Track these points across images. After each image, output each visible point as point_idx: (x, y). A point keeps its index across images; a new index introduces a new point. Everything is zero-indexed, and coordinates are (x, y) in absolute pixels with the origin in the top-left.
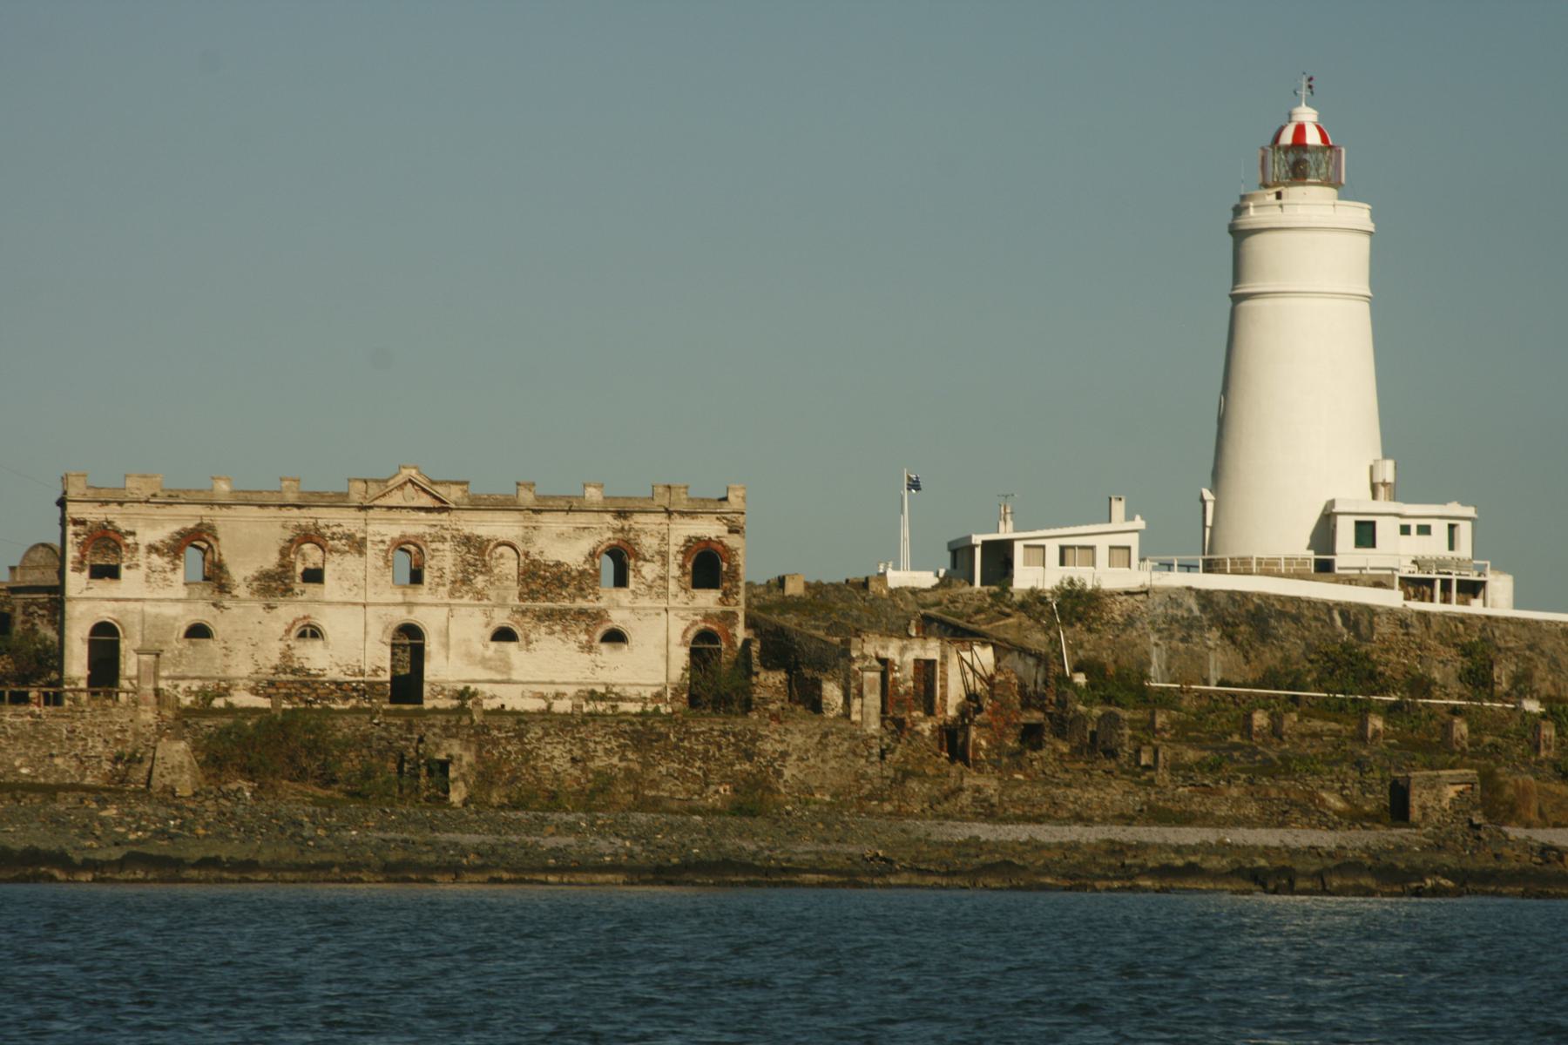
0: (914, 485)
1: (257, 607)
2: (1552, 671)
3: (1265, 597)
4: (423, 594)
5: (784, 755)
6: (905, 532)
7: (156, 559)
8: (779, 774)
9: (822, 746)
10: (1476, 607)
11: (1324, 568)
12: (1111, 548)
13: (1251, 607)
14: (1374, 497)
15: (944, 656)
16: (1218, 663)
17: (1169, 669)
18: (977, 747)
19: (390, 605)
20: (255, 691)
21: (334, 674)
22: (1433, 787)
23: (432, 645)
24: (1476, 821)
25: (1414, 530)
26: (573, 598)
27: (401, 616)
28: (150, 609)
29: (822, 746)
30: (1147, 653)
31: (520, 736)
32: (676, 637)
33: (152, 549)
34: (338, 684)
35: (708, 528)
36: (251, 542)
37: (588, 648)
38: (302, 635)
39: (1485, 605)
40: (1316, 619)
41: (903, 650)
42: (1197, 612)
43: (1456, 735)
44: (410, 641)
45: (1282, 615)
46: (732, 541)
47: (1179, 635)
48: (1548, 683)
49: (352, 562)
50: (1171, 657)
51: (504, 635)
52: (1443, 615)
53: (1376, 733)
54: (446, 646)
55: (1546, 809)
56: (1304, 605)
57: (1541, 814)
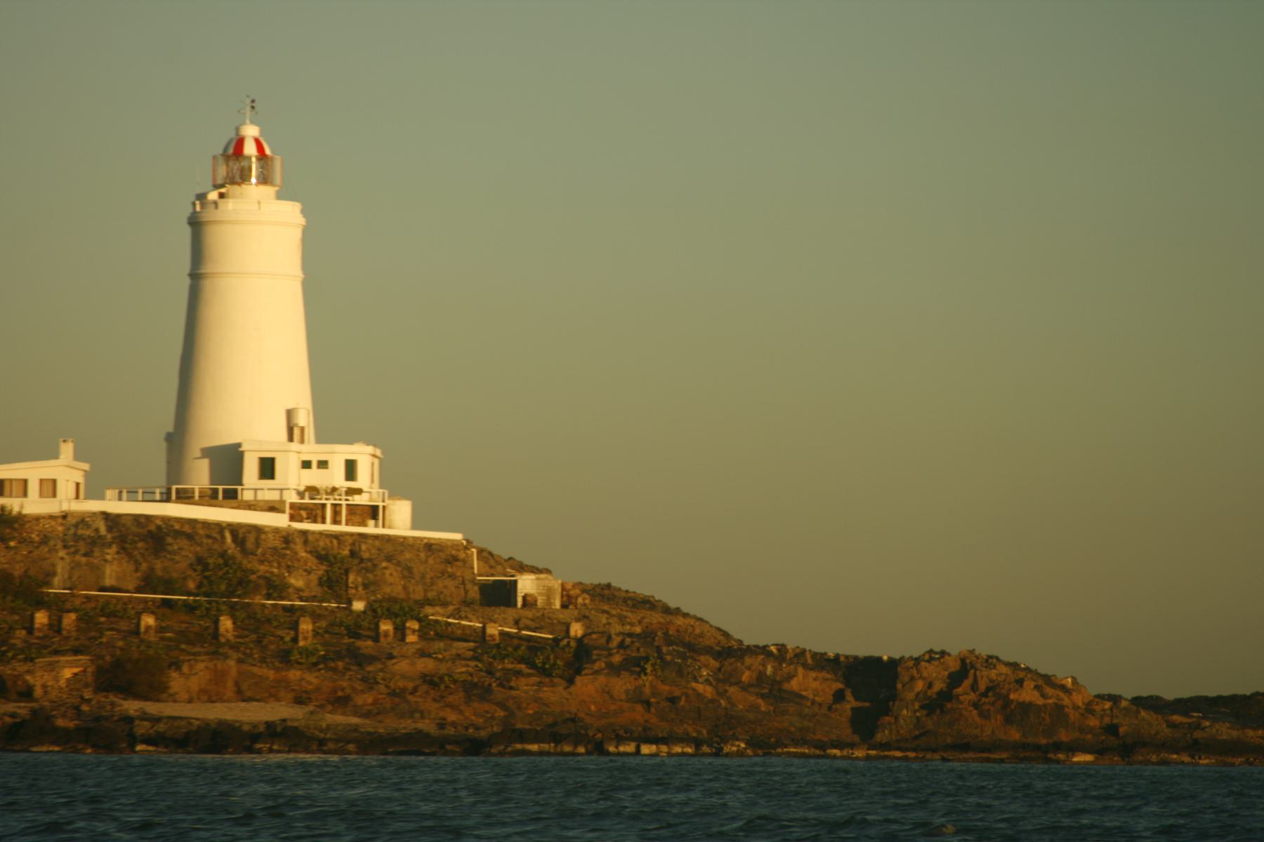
2: (404, 577)
3: (167, 520)
10: (371, 529)
11: (231, 496)
12: (54, 481)
13: (152, 528)
14: (291, 439)
16: (114, 569)
17: (70, 578)
22: (52, 670)
24: (87, 696)
25: (314, 465)
30: (54, 565)
39: (376, 526)
40: (208, 537)
42: (103, 530)
43: (222, 629)
45: (178, 534)
47: (82, 552)
48: (400, 587)
50: (72, 568)
52: (376, 537)
53: (148, 628)
55: (244, 687)
56: (199, 526)
57: (239, 692)
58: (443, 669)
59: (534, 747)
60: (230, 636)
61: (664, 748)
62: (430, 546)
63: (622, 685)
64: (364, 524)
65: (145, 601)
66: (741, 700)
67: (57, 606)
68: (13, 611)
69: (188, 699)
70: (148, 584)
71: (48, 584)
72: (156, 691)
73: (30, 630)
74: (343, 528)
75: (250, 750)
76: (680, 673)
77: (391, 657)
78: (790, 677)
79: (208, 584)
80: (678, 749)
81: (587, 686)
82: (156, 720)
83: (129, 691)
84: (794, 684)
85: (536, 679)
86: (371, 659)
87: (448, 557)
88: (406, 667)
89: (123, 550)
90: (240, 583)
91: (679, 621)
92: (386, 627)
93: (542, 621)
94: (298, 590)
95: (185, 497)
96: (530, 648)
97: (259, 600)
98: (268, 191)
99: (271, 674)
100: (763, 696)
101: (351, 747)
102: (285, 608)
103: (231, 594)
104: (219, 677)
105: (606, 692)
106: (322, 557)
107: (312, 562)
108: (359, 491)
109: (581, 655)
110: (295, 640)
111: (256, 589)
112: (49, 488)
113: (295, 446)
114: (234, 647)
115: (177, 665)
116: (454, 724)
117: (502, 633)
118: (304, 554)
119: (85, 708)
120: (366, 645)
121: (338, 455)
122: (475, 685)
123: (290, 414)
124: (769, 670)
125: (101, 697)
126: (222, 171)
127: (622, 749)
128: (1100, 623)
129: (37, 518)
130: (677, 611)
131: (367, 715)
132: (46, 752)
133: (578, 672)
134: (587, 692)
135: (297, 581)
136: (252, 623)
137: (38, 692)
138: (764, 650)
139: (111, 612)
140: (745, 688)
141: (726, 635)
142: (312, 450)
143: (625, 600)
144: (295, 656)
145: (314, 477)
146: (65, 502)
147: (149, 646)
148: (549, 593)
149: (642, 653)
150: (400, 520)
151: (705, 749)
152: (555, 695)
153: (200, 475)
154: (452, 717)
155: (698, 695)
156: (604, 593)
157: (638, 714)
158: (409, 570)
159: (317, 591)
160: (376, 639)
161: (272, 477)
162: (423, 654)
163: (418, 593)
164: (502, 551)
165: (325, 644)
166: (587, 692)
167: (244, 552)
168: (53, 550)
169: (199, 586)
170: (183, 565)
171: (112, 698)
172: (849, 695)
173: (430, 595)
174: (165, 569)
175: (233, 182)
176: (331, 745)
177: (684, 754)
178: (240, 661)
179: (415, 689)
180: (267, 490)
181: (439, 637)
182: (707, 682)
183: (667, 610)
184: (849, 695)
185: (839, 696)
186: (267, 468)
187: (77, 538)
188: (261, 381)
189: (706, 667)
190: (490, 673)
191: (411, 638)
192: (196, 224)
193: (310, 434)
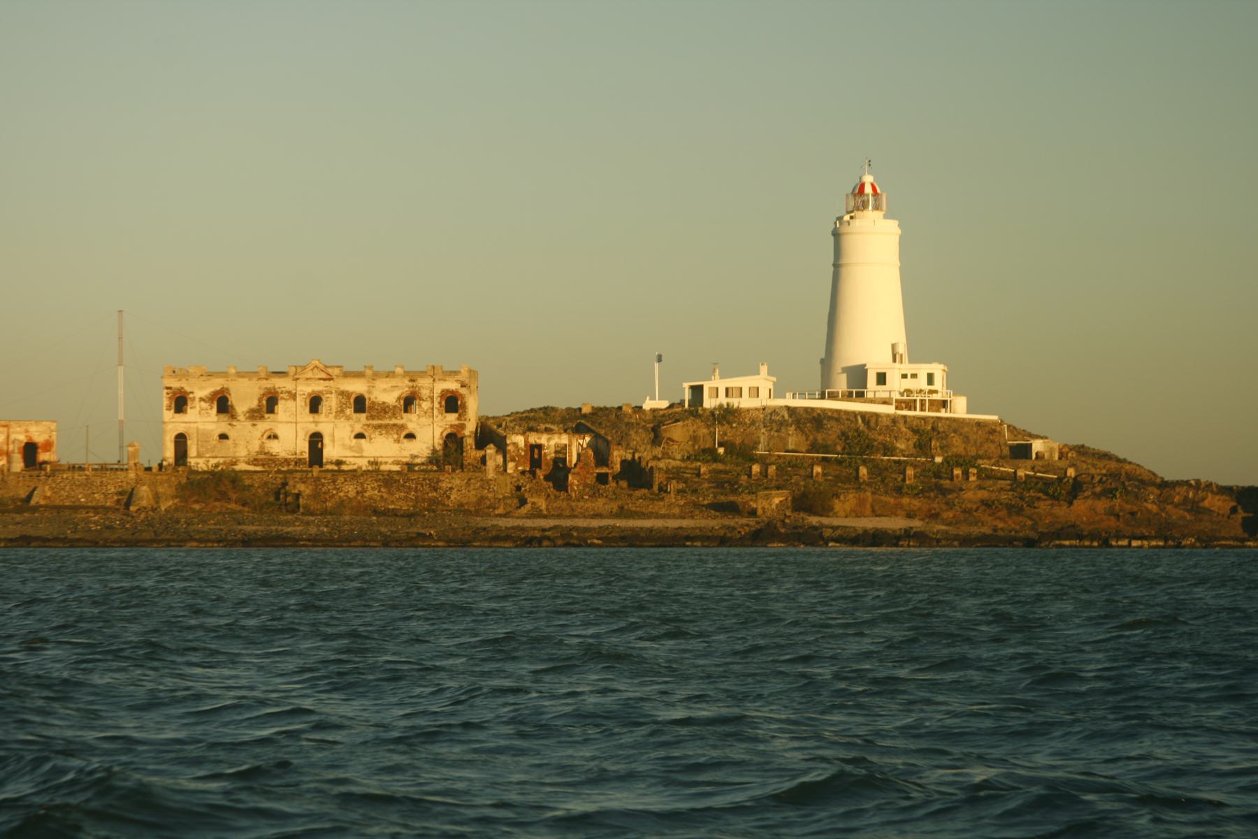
0: (660, 359)
1: (249, 424)
3: (824, 410)
4: (321, 417)
5: (451, 489)
6: (121, 392)
7: (204, 405)
8: (449, 497)
9: (468, 484)
11: (861, 395)
14: (894, 361)
15: (570, 441)
16: (793, 439)
18: (572, 484)
19: (308, 424)
20: (248, 463)
21: (283, 455)
23: (326, 440)
26: (390, 418)
27: (313, 428)
28: (201, 426)
29: (468, 484)
31: (334, 482)
32: (437, 435)
33: (202, 399)
34: (286, 460)
35: (452, 385)
36: (245, 396)
37: (398, 441)
38: (269, 437)
41: (549, 440)
42: (786, 417)
44: (316, 440)
45: (830, 418)
46: (463, 391)
49: (291, 403)
51: (360, 436)
52: (947, 419)
54: (333, 441)
55: (876, 508)
57: (873, 511)
58: (993, 496)
59: (1067, 543)
60: (866, 478)
61: (1146, 543)
62: (979, 424)
63: (1102, 505)
64: (938, 411)
65: (813, 458)
66: (1175, 514)
67: (763, 461)
68: (737, 465)
69: (846, 514)
70: (814, 447)
71: (756, 449)
72: (826, 511)
73: (750, 476)
74: (927, 413)
75: (896, 545)
76: (1137, 497)
77: (961, 490)
78: (1203, 499)
79: (848, 447)
80: (1154, 543)
81: (1081, 506)
82: (835, 528)
83: (811, 511)
84: (1206, 504)
85: (1049, 502)
86: (951, 491)
87: (990, 430)
88: (972, 495)
89: (798, 428)
90: (868, 447)
91: (1127, 467)
92: (957, 472)
93: (1048, 468)
94: (902, 451)
95: (833, 396)
96: (1045, 484)
97: (879, 457)
98: (879, 214)
99: (892, 500)
100: (1188, 511)
101: (956, 543)
102: (895, 462)
103: (862, 453)
104: (862, 503)
105: (1092, 509)
106: (915, 431)
107: (910, 434)
108: (936, 392)
109: (1076, 488)
110: (904, 480)
111: (878, 450)
112: (755, 392)
113: (897, 365)
114: (869, 485)
115: (837, 496)
116: (1002, 529)
117: (1027, 476)
118: (904, 429)
119: (787, 521)
120: (946, 483)
121: (923, 370)
122: (1013, 506)
123: (893, 346)
124: (1191, 495)
125: (796, 514)
126: (852, 203)
127: (1120, 543)
128: (1183, 438)
129: (748, 410)
130: (1124, 461)
131: (950, 524)
132: (776, 547)
133: (1075, 497)
134: (1081, 509)
135: (901, 445)
136: (878, 471)
137: (760, 512)
138: (1187, 483)
139: (795, 465)
140: (1177, 506)
141: (1154, 474)
142: (908, 368)
143: (1093, 455)
144: (905, 490)
145: (909, 384)
146: (764, 400)
147: (820, 484)
148: (1051, 451)
149: (1113, 486)
150: (960, 409)
151: (1170, 543)
152: (1062, 511)
153: (841, 384)
154: (1001, 525)
155: (1149, 511)
156: (1081, 450)
157: (1113, 522)
158: (967, 438)
159: (913, 451)
160: (952, 479)
161: (884, 383)
162: (980, 488)
163: (973, 452)
164: (1020, 426)
165: (922, 482)
166: (1081, 509)
167: (869, 428)
168: (758, 428)
169: (844, 449)
170: (834, 437)
171: (802, 515)
172: (1240, 509)
173: (980, 452)
174: (823, 439)
175: (858, 209)
176: (944, 542)
177: (1157, 547)
178: (873, 493)
179: (977, 509)
180: (882, 392)
181: (988, 477)
182: (1153, 502)
183: (1119, 460)
184: (1240, 509)
185: (1234, 510)
186: (882, 378)
187: (772, 421)
188: (876, 327)
189: (1153, 494)
190: (1022, 498)
191: (972, 478)
192: (837, 235)
193: (905, 358)
